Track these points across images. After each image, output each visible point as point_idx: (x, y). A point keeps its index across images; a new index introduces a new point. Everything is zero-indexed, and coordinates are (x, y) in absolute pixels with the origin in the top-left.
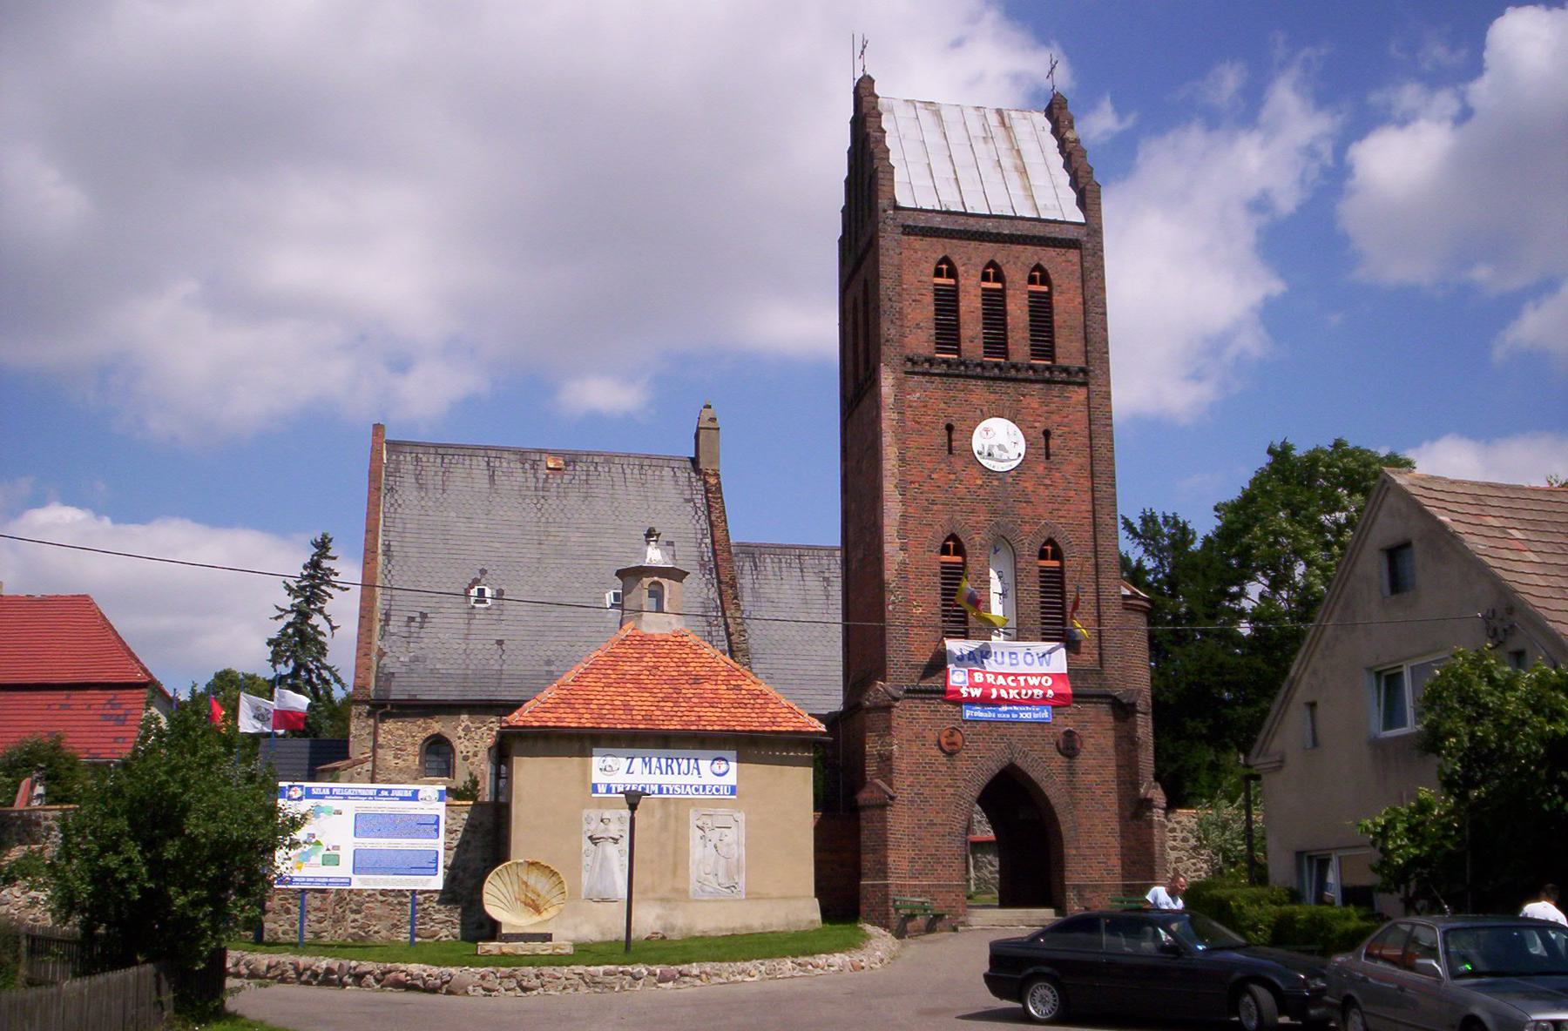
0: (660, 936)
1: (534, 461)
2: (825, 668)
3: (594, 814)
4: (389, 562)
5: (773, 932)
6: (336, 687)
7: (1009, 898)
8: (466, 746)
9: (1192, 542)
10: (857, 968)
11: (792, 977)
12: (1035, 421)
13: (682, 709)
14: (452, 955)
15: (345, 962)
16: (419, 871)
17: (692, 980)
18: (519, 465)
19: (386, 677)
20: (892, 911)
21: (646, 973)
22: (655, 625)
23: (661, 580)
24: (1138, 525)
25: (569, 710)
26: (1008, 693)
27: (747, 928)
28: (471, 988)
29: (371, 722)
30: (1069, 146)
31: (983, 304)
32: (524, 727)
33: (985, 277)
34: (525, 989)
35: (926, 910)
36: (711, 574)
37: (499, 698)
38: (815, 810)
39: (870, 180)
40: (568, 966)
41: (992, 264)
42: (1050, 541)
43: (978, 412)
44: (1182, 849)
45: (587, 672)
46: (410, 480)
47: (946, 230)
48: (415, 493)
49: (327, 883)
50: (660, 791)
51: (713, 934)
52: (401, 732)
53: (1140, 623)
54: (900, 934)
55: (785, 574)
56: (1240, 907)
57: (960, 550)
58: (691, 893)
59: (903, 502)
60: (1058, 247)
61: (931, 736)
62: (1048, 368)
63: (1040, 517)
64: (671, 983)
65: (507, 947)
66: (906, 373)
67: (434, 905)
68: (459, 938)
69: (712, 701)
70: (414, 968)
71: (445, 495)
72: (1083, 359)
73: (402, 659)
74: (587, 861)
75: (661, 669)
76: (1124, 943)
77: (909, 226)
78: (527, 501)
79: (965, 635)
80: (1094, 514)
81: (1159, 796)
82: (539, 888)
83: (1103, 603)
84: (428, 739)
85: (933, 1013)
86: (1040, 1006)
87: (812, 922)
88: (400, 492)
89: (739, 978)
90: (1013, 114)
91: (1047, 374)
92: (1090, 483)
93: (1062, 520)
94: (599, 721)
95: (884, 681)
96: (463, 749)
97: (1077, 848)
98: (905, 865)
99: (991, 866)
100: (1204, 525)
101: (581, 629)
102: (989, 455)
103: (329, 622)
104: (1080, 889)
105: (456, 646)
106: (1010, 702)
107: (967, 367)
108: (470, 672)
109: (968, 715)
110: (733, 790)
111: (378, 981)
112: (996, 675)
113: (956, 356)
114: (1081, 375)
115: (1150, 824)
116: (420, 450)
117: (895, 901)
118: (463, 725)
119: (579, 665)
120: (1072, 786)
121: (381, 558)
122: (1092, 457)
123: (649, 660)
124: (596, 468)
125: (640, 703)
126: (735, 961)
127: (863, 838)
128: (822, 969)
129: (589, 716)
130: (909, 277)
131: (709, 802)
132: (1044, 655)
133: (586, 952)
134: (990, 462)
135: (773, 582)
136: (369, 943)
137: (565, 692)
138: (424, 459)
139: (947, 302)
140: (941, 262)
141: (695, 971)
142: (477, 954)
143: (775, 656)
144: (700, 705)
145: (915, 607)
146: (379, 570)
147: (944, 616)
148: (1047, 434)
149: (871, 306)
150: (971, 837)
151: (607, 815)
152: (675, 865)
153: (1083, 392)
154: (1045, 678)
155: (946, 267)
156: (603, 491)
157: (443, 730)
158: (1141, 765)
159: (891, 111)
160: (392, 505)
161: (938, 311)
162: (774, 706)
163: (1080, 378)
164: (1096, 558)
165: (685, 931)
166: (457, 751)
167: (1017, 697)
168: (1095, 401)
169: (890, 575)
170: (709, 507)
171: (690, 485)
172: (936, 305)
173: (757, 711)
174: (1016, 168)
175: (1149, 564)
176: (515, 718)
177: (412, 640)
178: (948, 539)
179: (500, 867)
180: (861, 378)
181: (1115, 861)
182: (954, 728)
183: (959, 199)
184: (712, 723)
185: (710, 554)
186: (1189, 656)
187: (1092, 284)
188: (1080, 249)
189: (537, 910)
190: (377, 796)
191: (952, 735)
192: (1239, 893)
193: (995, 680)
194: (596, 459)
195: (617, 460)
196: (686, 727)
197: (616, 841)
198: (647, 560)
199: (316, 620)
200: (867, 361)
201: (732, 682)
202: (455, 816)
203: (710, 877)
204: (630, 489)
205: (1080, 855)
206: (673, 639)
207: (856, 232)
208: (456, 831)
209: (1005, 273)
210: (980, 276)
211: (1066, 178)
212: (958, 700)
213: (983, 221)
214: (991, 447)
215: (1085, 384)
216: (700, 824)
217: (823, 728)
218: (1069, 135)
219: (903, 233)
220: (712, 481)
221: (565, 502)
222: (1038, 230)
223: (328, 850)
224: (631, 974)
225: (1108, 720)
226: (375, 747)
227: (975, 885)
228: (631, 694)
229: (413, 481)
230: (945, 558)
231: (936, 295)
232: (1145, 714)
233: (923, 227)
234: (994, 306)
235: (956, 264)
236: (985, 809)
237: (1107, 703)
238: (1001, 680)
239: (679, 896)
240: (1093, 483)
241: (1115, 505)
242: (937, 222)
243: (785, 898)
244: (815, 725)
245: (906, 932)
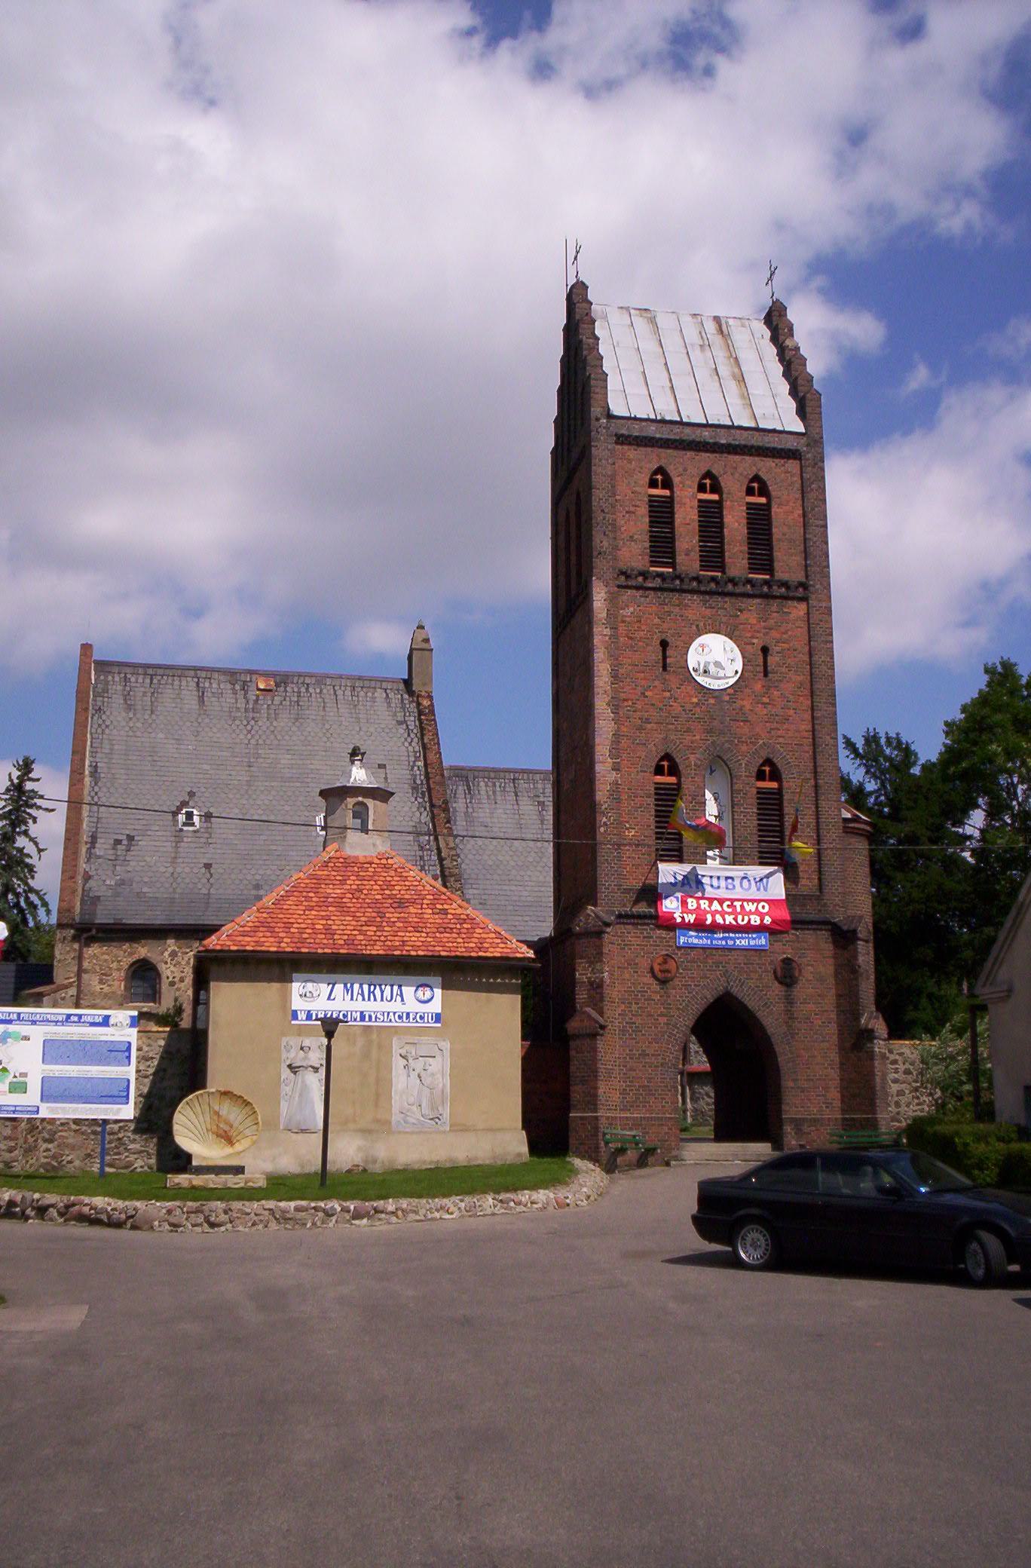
0: (361, 1168)
1: (244, 682)
2: (540, 894)
3: (294, 1041)
4: (96, 784)
5: (478, 1166)
6: (41, 912)
7: (727, 1130)
8: (172, 972)
9: (914, 763)
10: (561, 1205)
11: (493, 1214)
12: (753, 637)
13: (385, 934)
14: (141, 1187)
15: (28, 1194)
16: (110, 1099)
17: (388, 1217)
18: (229, 686)
19: (91, 901)
20: (602, 1144)
21: (339, 1209)
22: (359, 846)
23: (365, 801)
24: (860, 744)
25: (269, 934)
26: (724, 920)
27: (451, 1160)
28: (156, 1223)
29: (76, 946)
30: (788, 355)
31: (699, 516)
32: (221, 951)
33: (702, 488)
34: (212, 1225)
35: (637, 1144)
36: (423, 798)
37: (206, 923)
38: (524, 1038)
39: (583, 389)
40: (258, 1201)
41: (708, 475)
42: (768, 762)
43: (694, 627)
44: (904, 1082)
45: (289, 894)
46: (118, 700)
47: (661, 439)
48: (124, 714)
49: (14, 1112)
50: (363, 1018)
51: (416, 1167)
52: (106, 957)
53: (861, 847)
54: (610, 1168)
55: (499, 798)
56: (966, 1145)
57: (674, 770)
58: (393, 1123)
59: (616, 721)
60: (777, 458)
61: (644, 964)
62: (766, 582)
63: (757, 736)
64: (365, 1220)
65: (198, 1180)
66: (619, 586)
67: (130, 1134)
68: (155, 1168)
69: (416, 925)
70: (99, 1201)
71: (154, 717)
72: (803, 573)
73: (108, 882)
74: (286, 1089)
75: (365, 892)
76: (841, 1183)
77: (622, 435)
78: (237, 722)
79: (680, 860)
80: (814, 735)
81: (880, 1027)
82: (232, 1117)
83: (823, 826)
84: (134, 963)
85: (641, 1255)
86: (751, 1250)
87: (519, 1155)
88: (108, 713)
89: (437, 1215)
90: (731, 322)
91: (765, 589)
92: (809, 702)
93: (781, 740)
94: (298, 945)
95: (595, 905)
96: (169, 974)
97: (795, 1080)
98: (616, 1097)
99: (707, 1097)
100: (929, 747)
101: (291, 853)
102: (705, 672)
103: (36, 844)
104: (798, 1123)
105: (163, 869)
106: (727, 928)
107: (682, 580)
108: (177, 896)
109: (682, 941)
110: (438, 1018)
111: (61, 1214)
112: (711, 900)
113: (671, 570)
114: (801, 590)
115: (871, 1056)
116: (128, 670)
117: (604, 1134)
118: (170, 949)
119: (279, 888)
120: (790, 1016)
121: (87, 780)
122: (811, 674)
123: (352, 882)
124: (307, 689)
125: (342, 927)
126: (434, 1197)
127: (572, 1068)
128: (525, 1206)
129: (289, 940)
130: (622, 488)
131: (411, 1030)
132: (761, 880)
133: (280, 1186)
134: (706, 679)
135: (487, 805)
136: (61, 1173)
137: (265, 915)
138: (133, 679)
139: (662, 513)
140: (656, 472)
141: (391, 1208)
142: (166, 1187)
143: (488, 882)
144: (405, 929)
145: (627, 829)
146: (86, 791)
147: (657, 839)
148: (765, 650)
149: (584, 518)
150: (689, 1068)
151: (307, 1042)
152: (378, 1096)
153: (802, 607)
154: (762, 903)
155: (661, 478)
156: (314, 713)
157: (149, 955)
158: (862, 994)
159: (605, 318)
160: (100, 726)
161: (652, 524)
162: (481, 931)
163: (800, 592)
164: (816, 779)
166: (164, 976)
167: (734, 923)
168: (816, 616)
169: (601, 795)
170: (422, 729)
171: (403, 707)
172: (650, 516)
173: (464, 936)
174: (734, 377)
175: (871, 786)
176: (213, 942)
177: (118, 862)
178: (662, 759)
179: (190, 1097)
180: (573, 593)
181: (834, 1095)
182: (667, 955)
183: (676, 410)
184: (416, 948)
185: (422, 777)
186: (912, 882)
187: (811, 496)
188: (800, 459)
189: (230, 1141)
190: (66, 1021)
191: (665, 962)
192: (965, 1130)
193: (710, 906)
194: (308, 680)
195: (328, 682)
196: (390, 953)
197: (316, 1070)
198: (352, 780)
199: (21, 842)
200: (579, 574)
201: (438, 906)
202: (152, 1043)
203: (414, 1108)
204: (341, 710)
205: (798, 1088)
206: (378, 862)
207: (568, 443)
208: (152, 1058)
209: (722, 484)
210: (696, 487)
211: (785, 387)
212: (669, 925)
213: (699, 431)
214: (707, 664)
215: (804, 599)
217: (531, 954)
218: (788, 343)
219: (617, 443)
220: (426, 703)
221: (275, 723)
222: (756, 440)
223: (15, 1077)
224: (324, 1211)
225: (827, 947)
226: (80, 971)
227: (692, 1116)
228: (332, 918)
229: (122, 702)
230: (659, 779)
231: (650, 506)
232: (867, 941)
233: (637, 437)
234: (711, 518)
235: (671, 474)
236: (701, 1042)
237: (825, 930)
238: (716, 906)
239: (381, 1127)
240: (812, 702)
241: (836, 725)
242: (652, 431)
243: (491, 1130)
244: (523, 950)
245: (616, 1167)
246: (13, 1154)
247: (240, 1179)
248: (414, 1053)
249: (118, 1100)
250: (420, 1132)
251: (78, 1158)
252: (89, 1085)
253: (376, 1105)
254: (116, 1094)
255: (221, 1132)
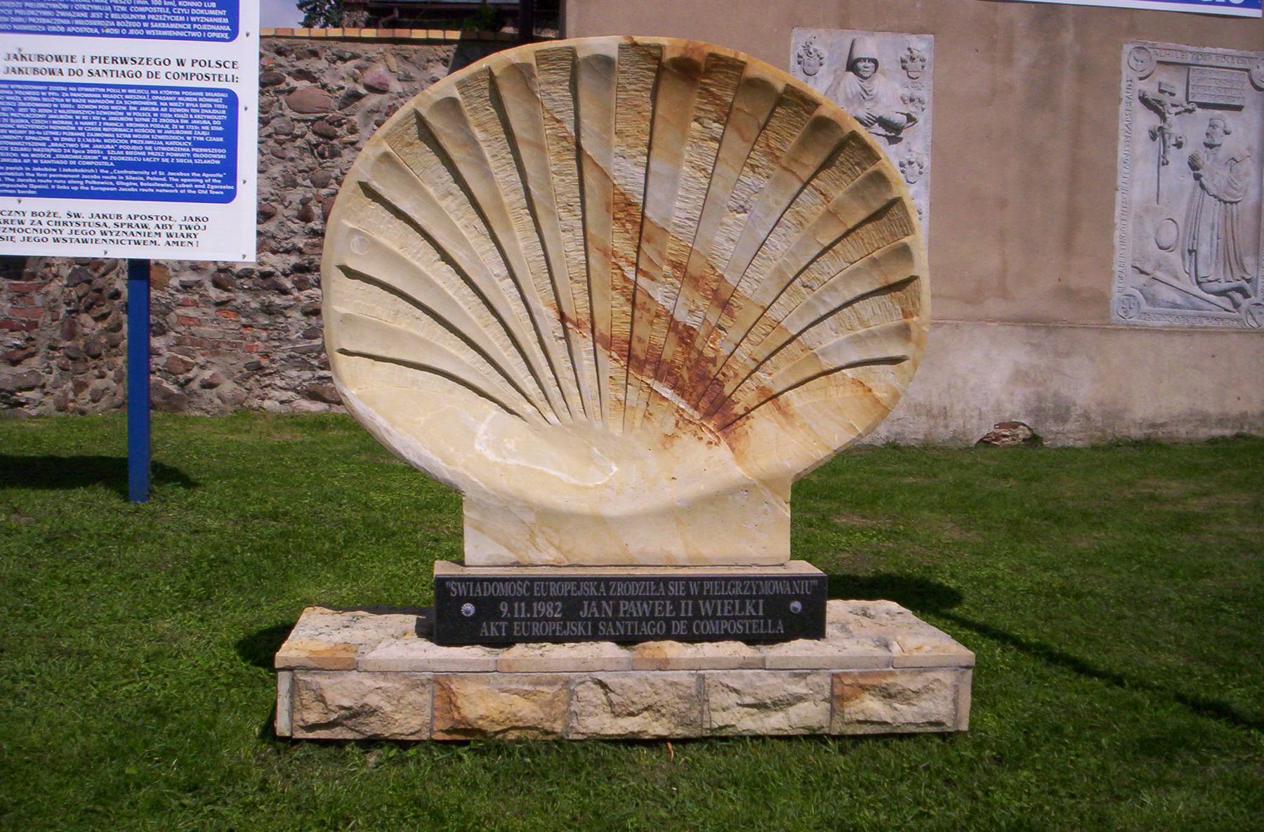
0: (1022, 433)
16: (156, 181)
51: (1182, 431)
58: (1116, 296)
151: (868, 47)
165: (1098, 421)
202: (413, 71)
203: (1175, 258)
216: (1151, 89)
246: (19, 369)
247: (800, 674)
248: (1180, 96)
249: (186, 183)
250: (1190, 332)
251: (230, 375)
252: (62, 123)
253: (1068, 244)
254: (180, 154)
255: (655, 335)
